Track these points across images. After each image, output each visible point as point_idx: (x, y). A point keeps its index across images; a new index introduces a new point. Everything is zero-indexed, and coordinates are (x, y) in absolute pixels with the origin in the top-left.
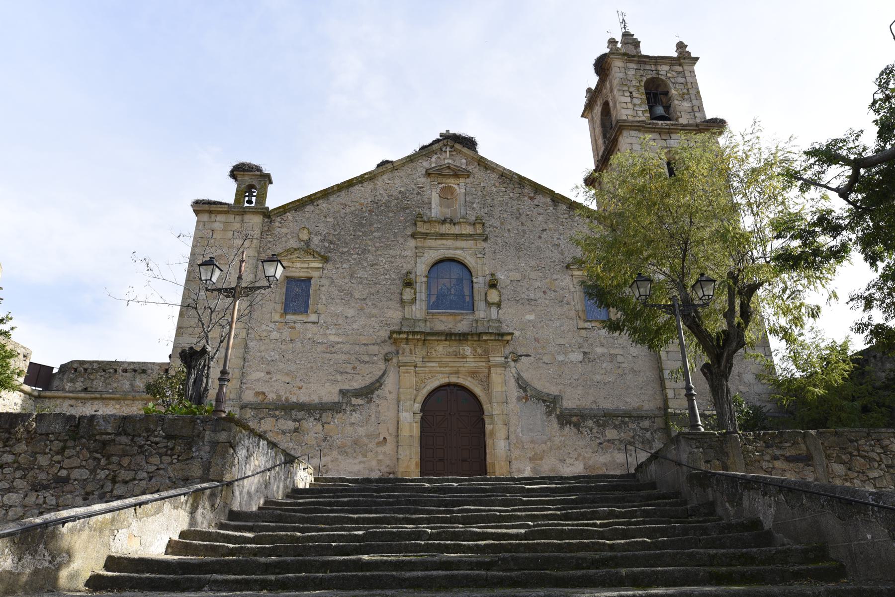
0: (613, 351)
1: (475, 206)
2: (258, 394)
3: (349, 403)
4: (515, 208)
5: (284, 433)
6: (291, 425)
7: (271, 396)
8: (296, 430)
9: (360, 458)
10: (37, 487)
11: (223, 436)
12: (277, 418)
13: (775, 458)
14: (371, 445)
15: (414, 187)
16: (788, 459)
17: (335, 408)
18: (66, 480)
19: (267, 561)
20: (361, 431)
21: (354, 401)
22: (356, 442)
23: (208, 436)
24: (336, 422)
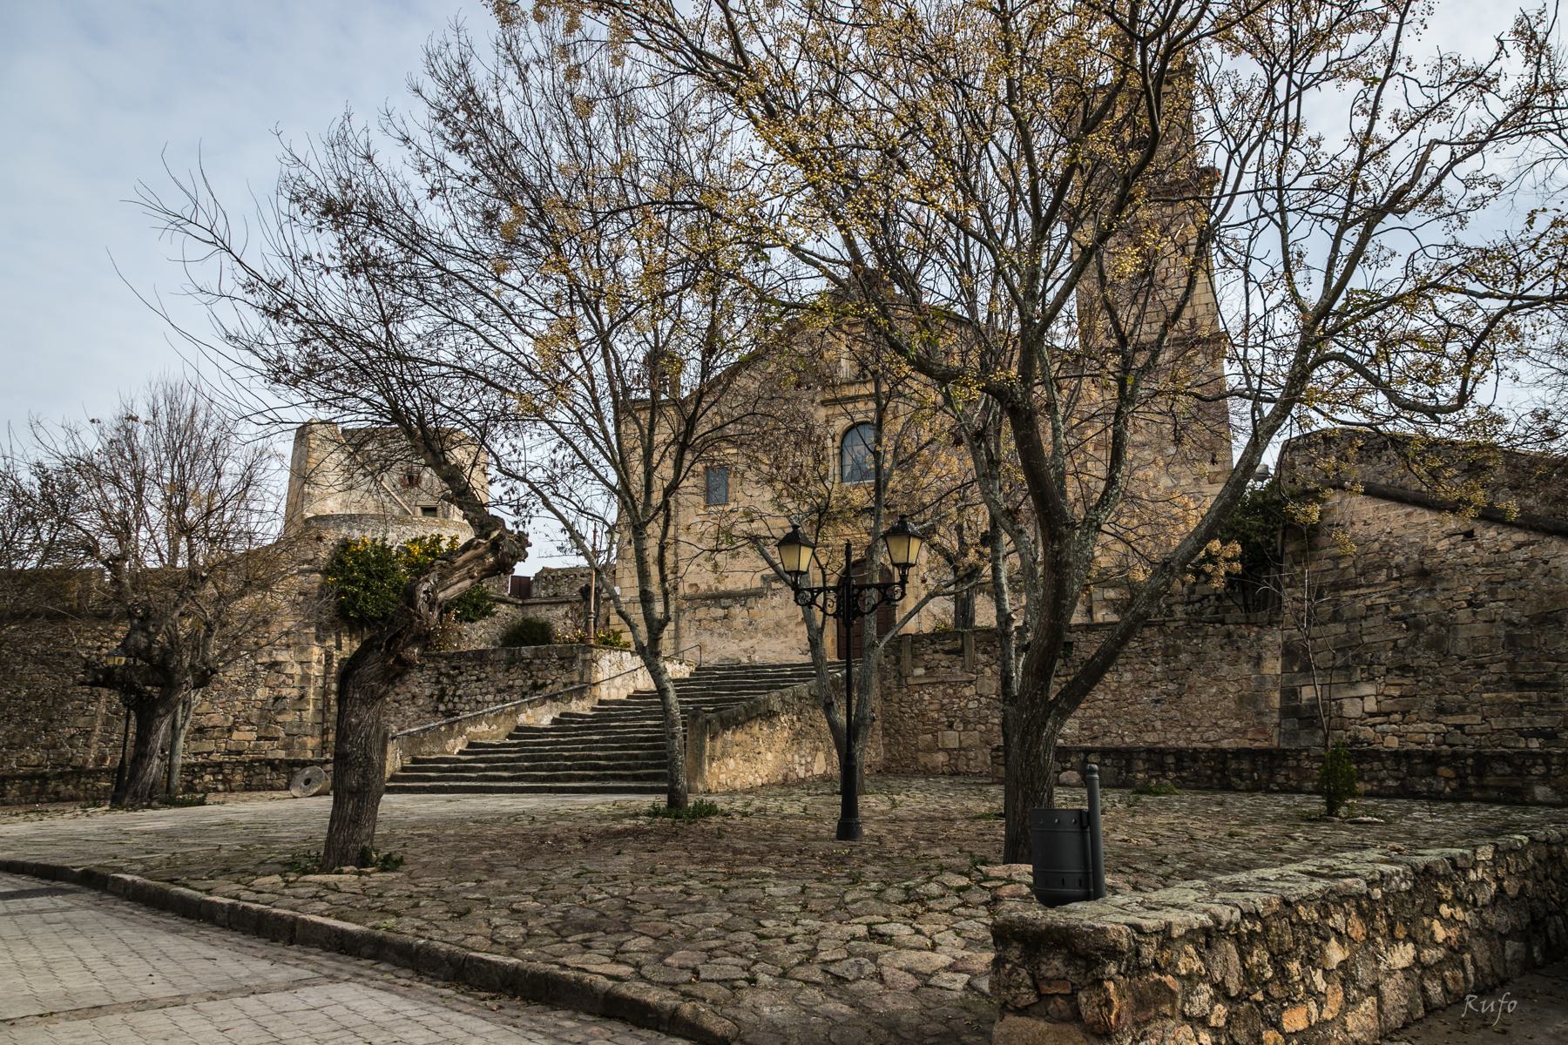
2: (691, 585)
3: (769, 587)
5: (715, 620)
6: (720, 612)
7: (703, 587)
8: (725, 617)
9: (782, 638)
10: (499, 691)
11: (588, 656)
12: (708, 607)
13: (936, 652)
14: (791, 626)
16: (947, 652)
17: (758, 594)
18: (511, 687)
19: (734, 733)
20: (782, 613)
21: (774, 585)
22: (778, 624)
23: (581, 656)
24: (759, 606)
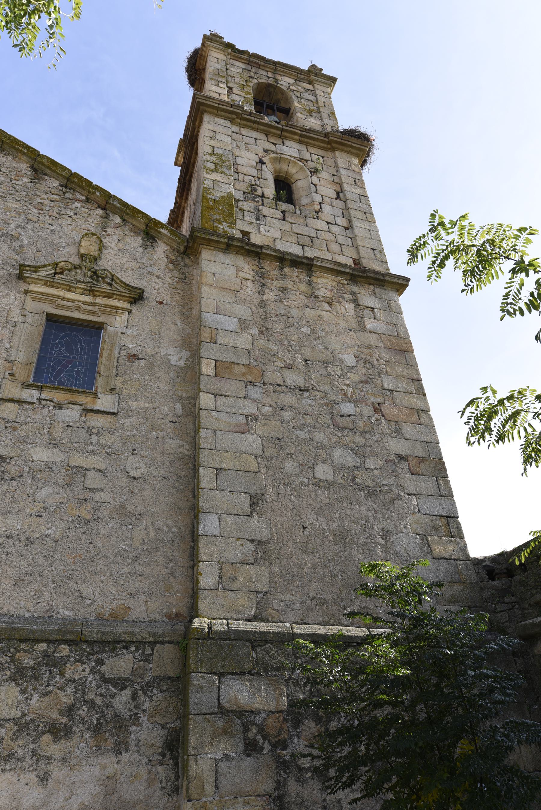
0: (78, 460)
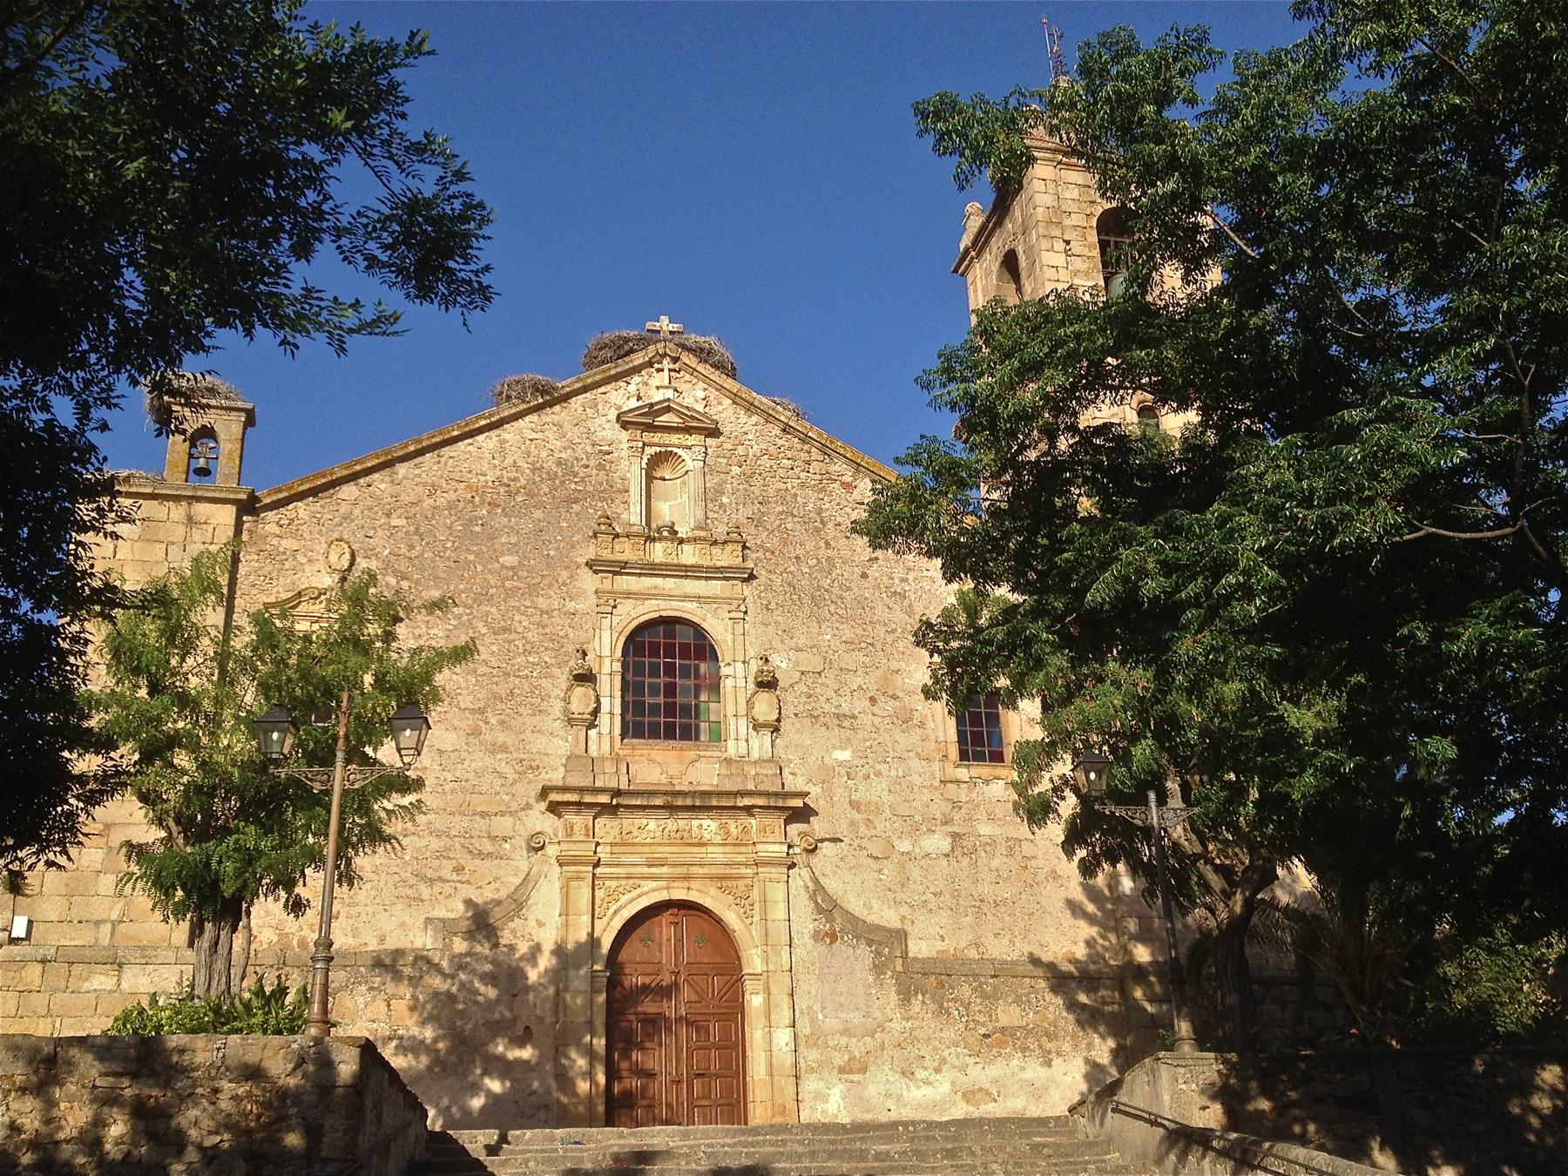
1: (725, 500)
4: (810, 507)
15: (589, 449)
